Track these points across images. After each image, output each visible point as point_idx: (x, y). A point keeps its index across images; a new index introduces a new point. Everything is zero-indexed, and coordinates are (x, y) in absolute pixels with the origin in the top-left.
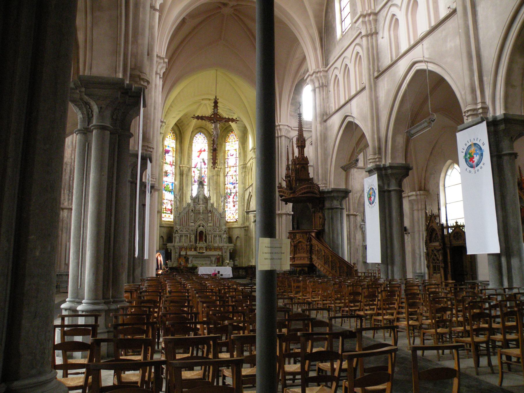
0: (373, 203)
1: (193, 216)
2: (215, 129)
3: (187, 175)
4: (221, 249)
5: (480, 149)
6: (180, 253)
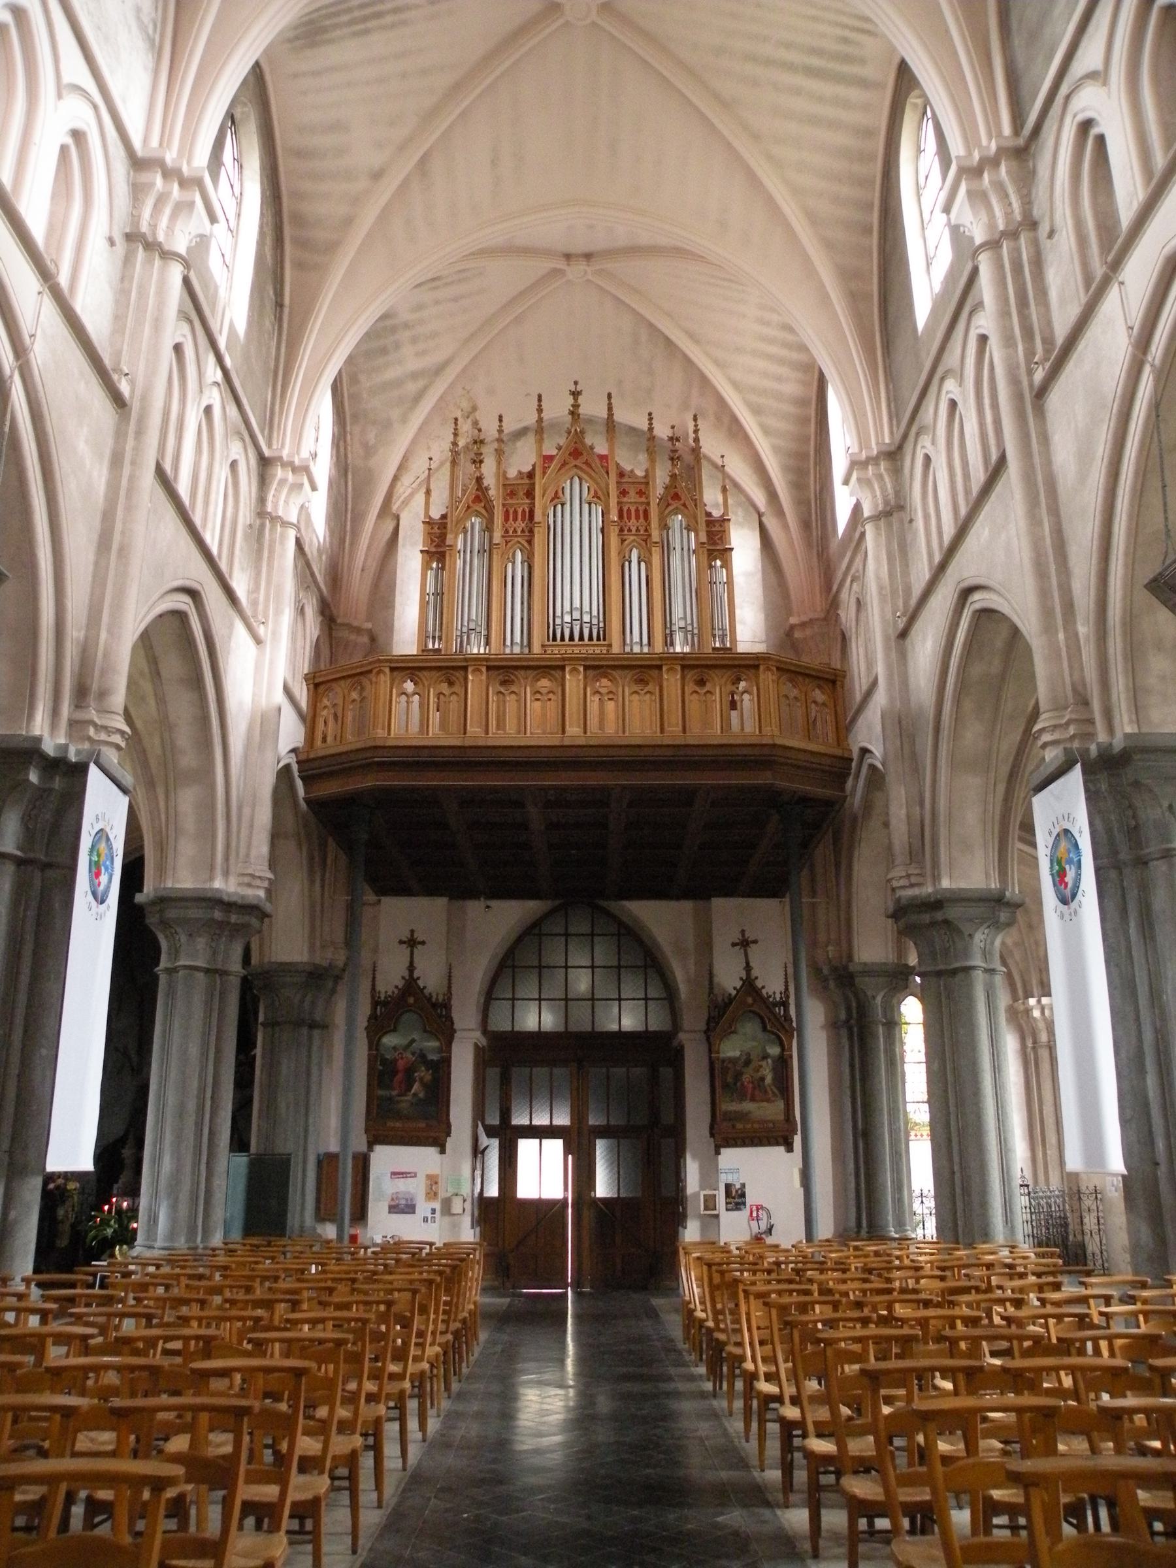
0: (1074, 896)
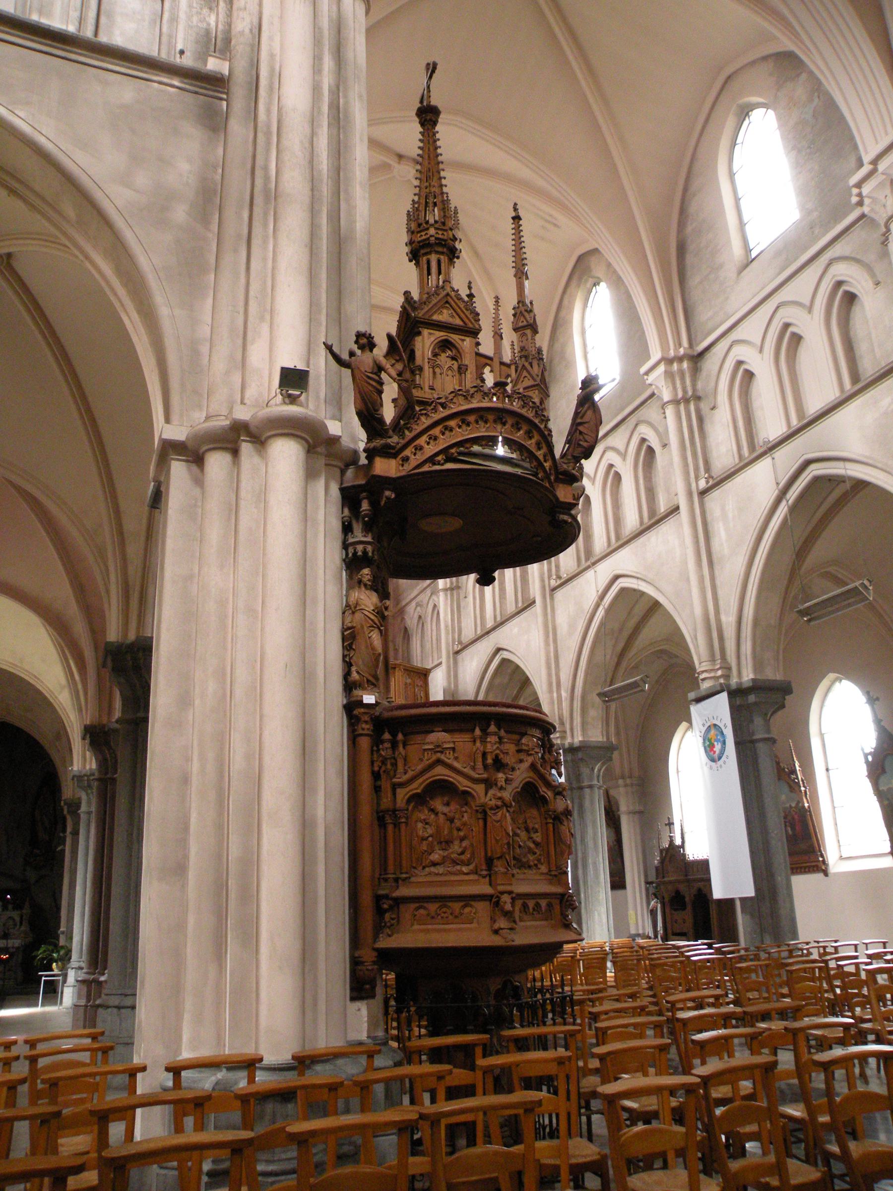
5: (722, 733)
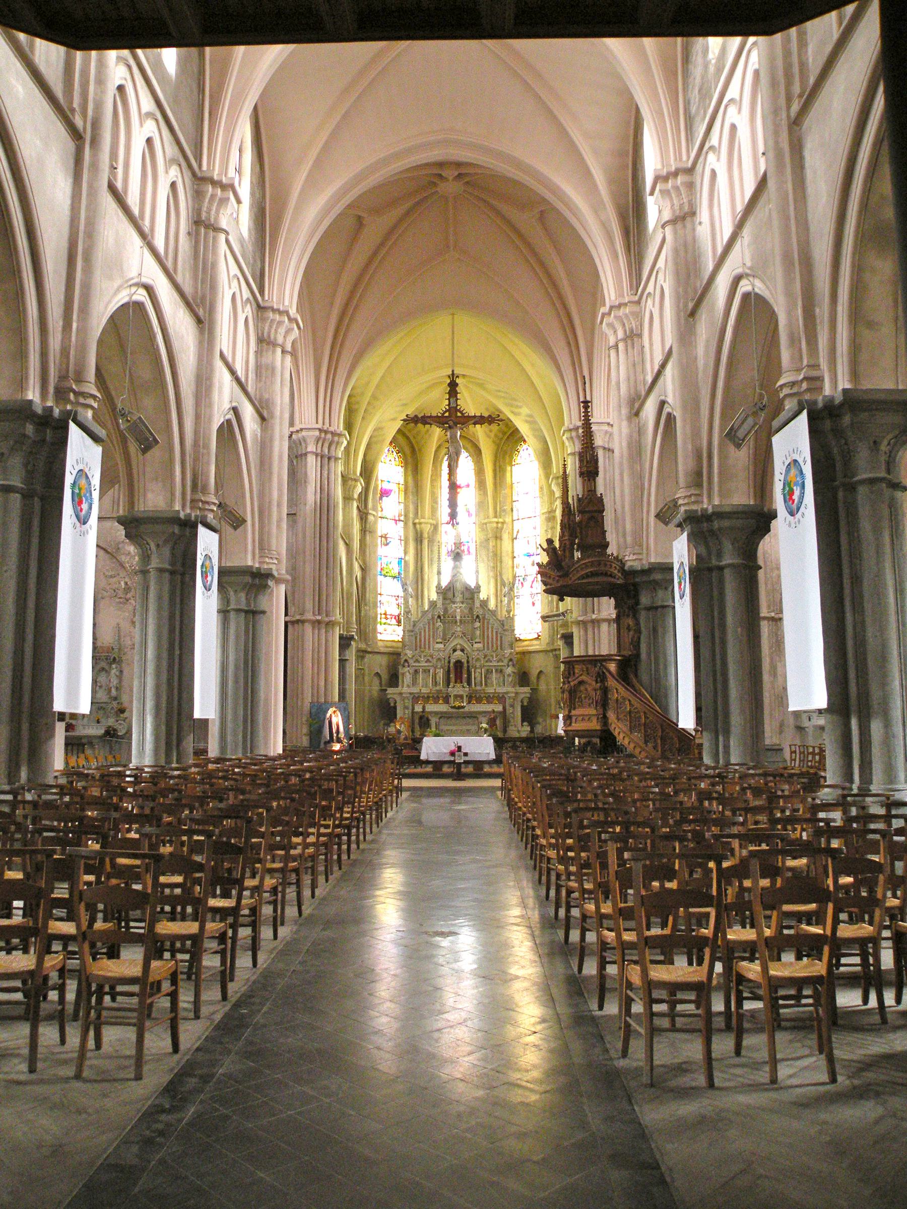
1: (441, 629)
2: (452, 442)
3: (431, 541)
4: (501, 699)
6: (413, 709)
